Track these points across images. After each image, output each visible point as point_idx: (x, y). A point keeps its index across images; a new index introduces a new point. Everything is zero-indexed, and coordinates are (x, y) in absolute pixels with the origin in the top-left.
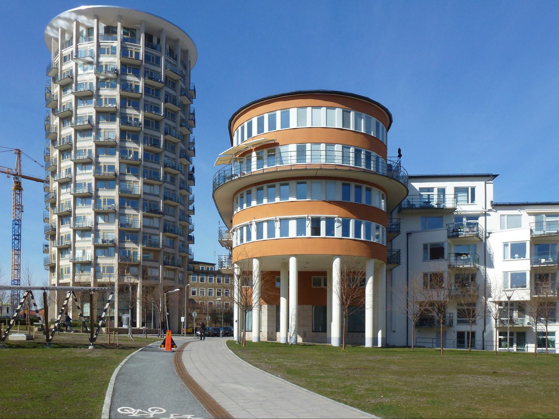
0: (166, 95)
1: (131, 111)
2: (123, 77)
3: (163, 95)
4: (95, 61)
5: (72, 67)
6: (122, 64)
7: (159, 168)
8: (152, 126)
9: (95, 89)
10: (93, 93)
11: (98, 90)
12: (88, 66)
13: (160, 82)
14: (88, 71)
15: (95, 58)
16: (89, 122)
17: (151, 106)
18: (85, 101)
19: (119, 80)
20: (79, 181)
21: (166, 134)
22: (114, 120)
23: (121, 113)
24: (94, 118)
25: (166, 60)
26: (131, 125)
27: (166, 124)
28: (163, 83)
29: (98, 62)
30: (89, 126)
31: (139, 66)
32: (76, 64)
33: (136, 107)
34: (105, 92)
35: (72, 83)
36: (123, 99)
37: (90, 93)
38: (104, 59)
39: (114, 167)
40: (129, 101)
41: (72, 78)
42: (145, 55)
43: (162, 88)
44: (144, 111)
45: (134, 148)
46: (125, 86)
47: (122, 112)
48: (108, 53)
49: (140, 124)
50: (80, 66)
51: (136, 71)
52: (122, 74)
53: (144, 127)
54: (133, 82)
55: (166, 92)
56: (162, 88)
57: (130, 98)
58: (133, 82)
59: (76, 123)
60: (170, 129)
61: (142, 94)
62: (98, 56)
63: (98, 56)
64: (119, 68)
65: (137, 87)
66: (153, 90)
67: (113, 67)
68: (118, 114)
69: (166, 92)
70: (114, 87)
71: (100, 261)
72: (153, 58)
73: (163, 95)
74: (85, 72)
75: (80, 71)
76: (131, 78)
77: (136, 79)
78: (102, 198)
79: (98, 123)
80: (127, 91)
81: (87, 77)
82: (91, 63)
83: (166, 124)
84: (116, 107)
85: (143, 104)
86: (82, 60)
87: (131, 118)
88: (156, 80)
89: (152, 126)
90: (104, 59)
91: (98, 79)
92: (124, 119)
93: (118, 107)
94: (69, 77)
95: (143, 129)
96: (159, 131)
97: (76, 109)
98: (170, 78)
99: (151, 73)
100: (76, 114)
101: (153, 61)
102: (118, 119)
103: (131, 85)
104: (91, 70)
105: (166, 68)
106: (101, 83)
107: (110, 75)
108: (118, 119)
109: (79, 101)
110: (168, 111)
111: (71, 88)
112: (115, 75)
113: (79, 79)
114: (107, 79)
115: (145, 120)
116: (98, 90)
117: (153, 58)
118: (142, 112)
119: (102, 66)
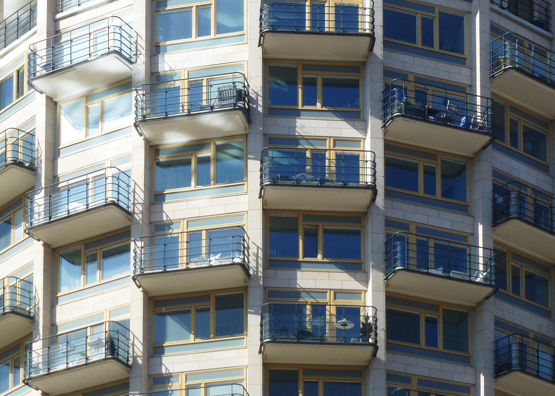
0: (496, 189)
1: (318, 279)
2: (279, 126)
3: (480, 192)
4: (140, 69)
5: (30, 265)
6: (272, 68)
7: (468, 379)
8: (432, 340)
9: (141, 196)
10: (130, 214)
11: (155, 198)
12: (111, 100)
13: (466, 128)
14: (109, 125)
15: (142, 58)
16: (112, 347)
17: (422, 246)
18: (91, 267)
19: (257, 142)
20: (66, 324)
21: (499, 216)
22: (233, 328)
23: (270, 293)
24: (137, 329)
25: (494, 30)
26: (322, 341)
27: (499, 323)
28: (481, 131)
29: (156, 80)
30: (114, 371)
31: (359, 67)
32: (52, 104)
33: (348, 258)
34: (192, 207)
35: (33, 189)
36: (278, 224)
37: (112, 220)
38: (182, 60)
39: (239, 233)
40: (309, 84)
41: (33, 169)
42: (388, 163)
43: (476, 308)
44: (388, 268)
45: (337, 293)
46: (289, 164)
47: (274, 284)
48: (203, 30)
49: (368, 329)
50: (69, 113)
51: (341, 92)
52: (271, 111)
53: (389, 348)
54: (329, 144)
55: (496, 173)
56: (475, 158)
57: (311, 216)
58: (329, 298)
59: (49, 361)
60: (522, 347)
61: (373, 188)
62: (154, 50)
63: (154, 50)
64: (256, 85)
65: (349, 164)
66: (432, 322)
67: (224, 82)
68: (256, 297)
69: (496, 173)
70: (234, 177)
71: (174, 209)
72: (427, 24)
73: (480, 192)
74: (94, 132)
75: (69, 133)
76: (318, 127)
77: (342, 128)
78: (179, 231)
79: (155, 348)
80: (298, 184)
81: (104, 153)
82: (123, 84)
83: (499, 323)
84: (244, 267)
85: (381, 239)
86: (84, 77)
87: (319, 310)
88: (448, 121)
89: (432, 340)
90: (182, 60)
91: (153, 149)
92: (287, 318)
93: (255, 263)
94: (18, 163)
95: (381, 354)
96: (466, 361)
97: (52, 299)
98: (516, 109)
99: (421, 95)
100: (52, 326)
101: (428, 40)
102: (254, 321)
103: (319, 156)
104: (124, 111)
105: (493, 63)
106: (166, 167)
107: (216, 121)
108: (254, 321)
109: (65, 267)
110: (510, 263)
111: (28, 214)
112: (239, 117)
113: (66, 166)
114: (198, 145)
115: (389, 313)
116: (155, 198)
117: (427, 24)
118: (374, 124)
119: (175, 240)
